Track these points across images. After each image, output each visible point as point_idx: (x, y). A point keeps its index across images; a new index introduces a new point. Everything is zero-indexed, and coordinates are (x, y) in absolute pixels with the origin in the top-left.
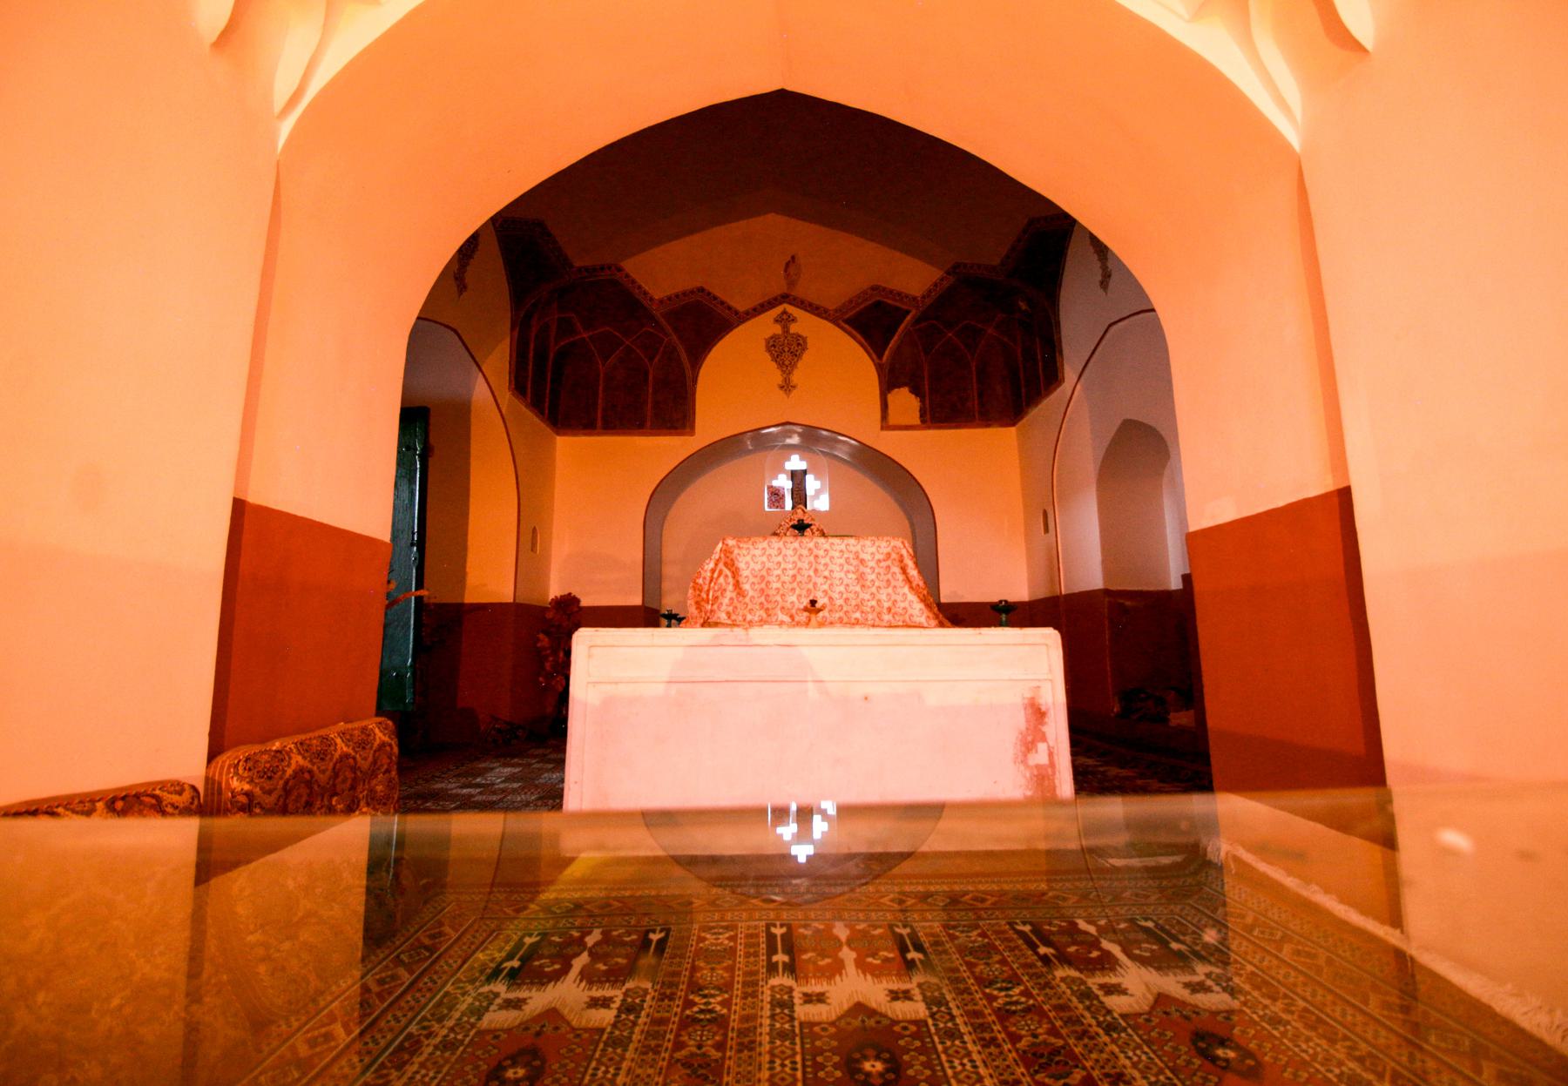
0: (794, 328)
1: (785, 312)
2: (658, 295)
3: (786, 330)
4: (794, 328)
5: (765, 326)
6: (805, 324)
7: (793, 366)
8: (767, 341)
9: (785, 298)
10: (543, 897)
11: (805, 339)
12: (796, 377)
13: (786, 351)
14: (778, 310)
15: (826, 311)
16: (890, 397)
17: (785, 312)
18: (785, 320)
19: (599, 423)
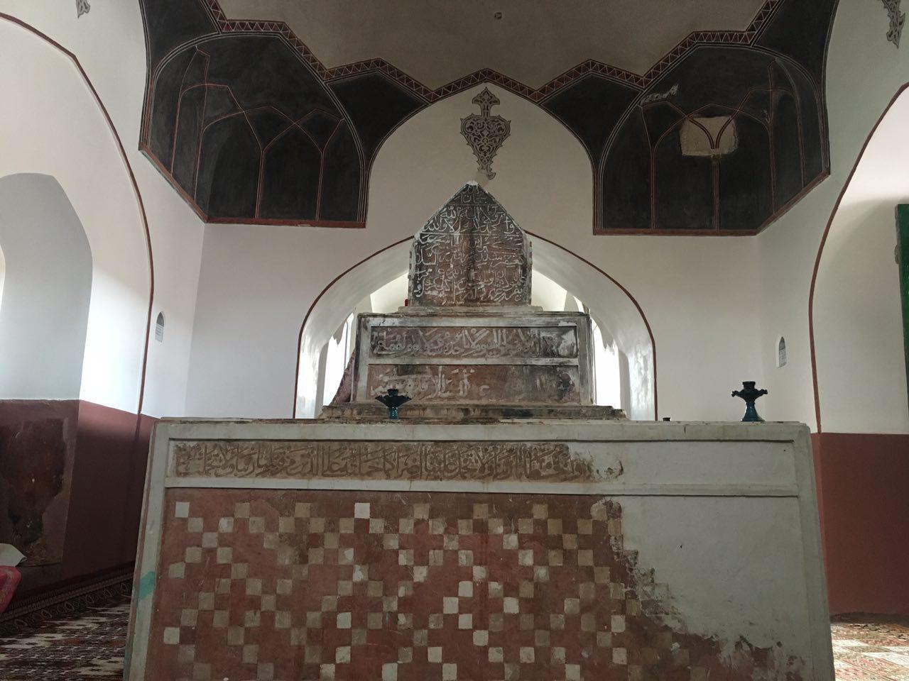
0: (495, 111)
1: (486, 92)
2: (743, 28)
3: (486, 110)
4: (495, 111)
5: (463, 105)
6: (509, 106)
7: (493, 150)
8: (464, 121)
9: (487, 75)
10: (286, 580)
11: (508, 124)
12: (495, 167)
13: (486, 136)
14: (478, 90)
15: (531, 92)
16: (433, 87)
17: (486, 92)
18: (487, 101)
19: (257, 215)
